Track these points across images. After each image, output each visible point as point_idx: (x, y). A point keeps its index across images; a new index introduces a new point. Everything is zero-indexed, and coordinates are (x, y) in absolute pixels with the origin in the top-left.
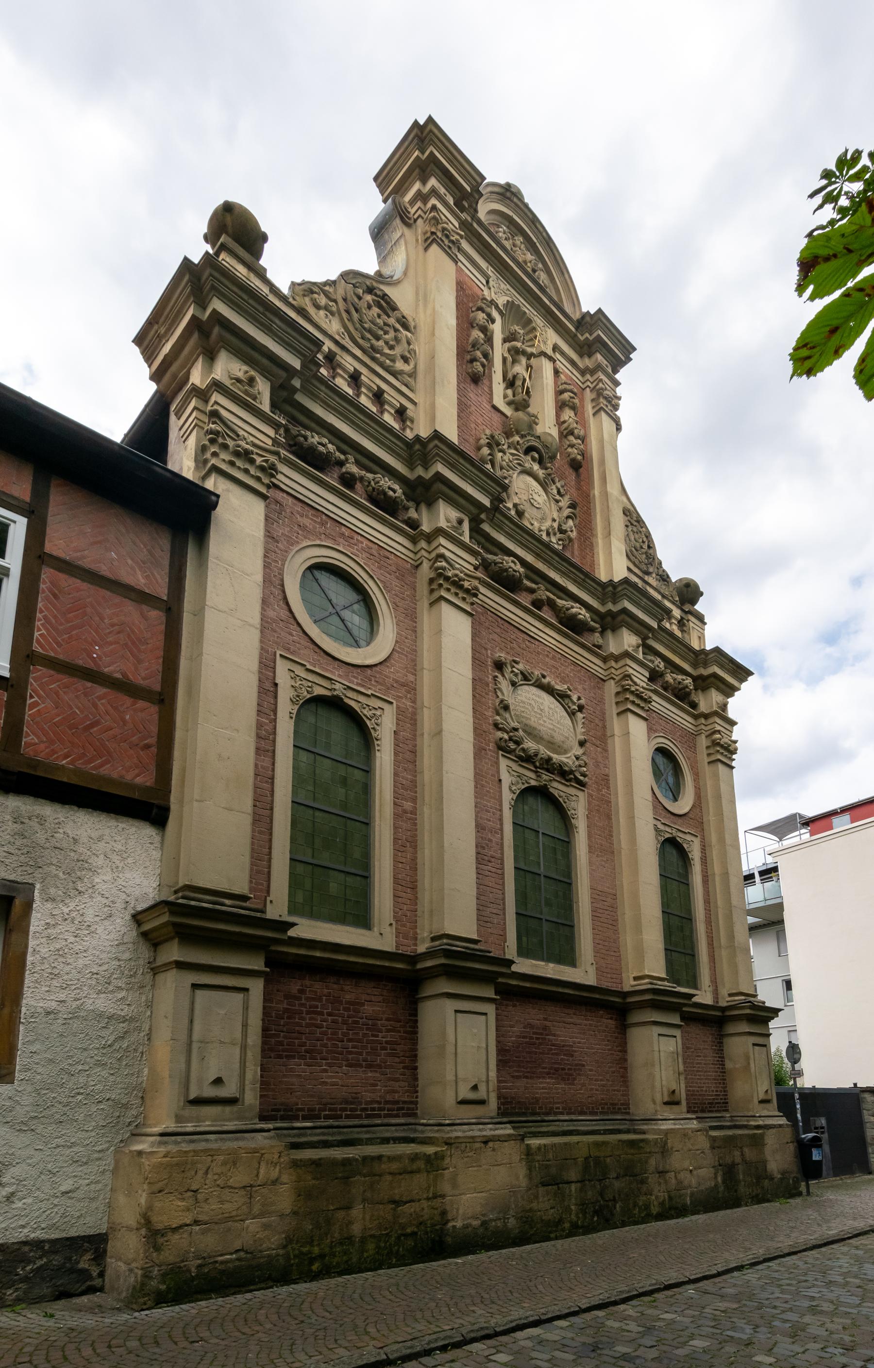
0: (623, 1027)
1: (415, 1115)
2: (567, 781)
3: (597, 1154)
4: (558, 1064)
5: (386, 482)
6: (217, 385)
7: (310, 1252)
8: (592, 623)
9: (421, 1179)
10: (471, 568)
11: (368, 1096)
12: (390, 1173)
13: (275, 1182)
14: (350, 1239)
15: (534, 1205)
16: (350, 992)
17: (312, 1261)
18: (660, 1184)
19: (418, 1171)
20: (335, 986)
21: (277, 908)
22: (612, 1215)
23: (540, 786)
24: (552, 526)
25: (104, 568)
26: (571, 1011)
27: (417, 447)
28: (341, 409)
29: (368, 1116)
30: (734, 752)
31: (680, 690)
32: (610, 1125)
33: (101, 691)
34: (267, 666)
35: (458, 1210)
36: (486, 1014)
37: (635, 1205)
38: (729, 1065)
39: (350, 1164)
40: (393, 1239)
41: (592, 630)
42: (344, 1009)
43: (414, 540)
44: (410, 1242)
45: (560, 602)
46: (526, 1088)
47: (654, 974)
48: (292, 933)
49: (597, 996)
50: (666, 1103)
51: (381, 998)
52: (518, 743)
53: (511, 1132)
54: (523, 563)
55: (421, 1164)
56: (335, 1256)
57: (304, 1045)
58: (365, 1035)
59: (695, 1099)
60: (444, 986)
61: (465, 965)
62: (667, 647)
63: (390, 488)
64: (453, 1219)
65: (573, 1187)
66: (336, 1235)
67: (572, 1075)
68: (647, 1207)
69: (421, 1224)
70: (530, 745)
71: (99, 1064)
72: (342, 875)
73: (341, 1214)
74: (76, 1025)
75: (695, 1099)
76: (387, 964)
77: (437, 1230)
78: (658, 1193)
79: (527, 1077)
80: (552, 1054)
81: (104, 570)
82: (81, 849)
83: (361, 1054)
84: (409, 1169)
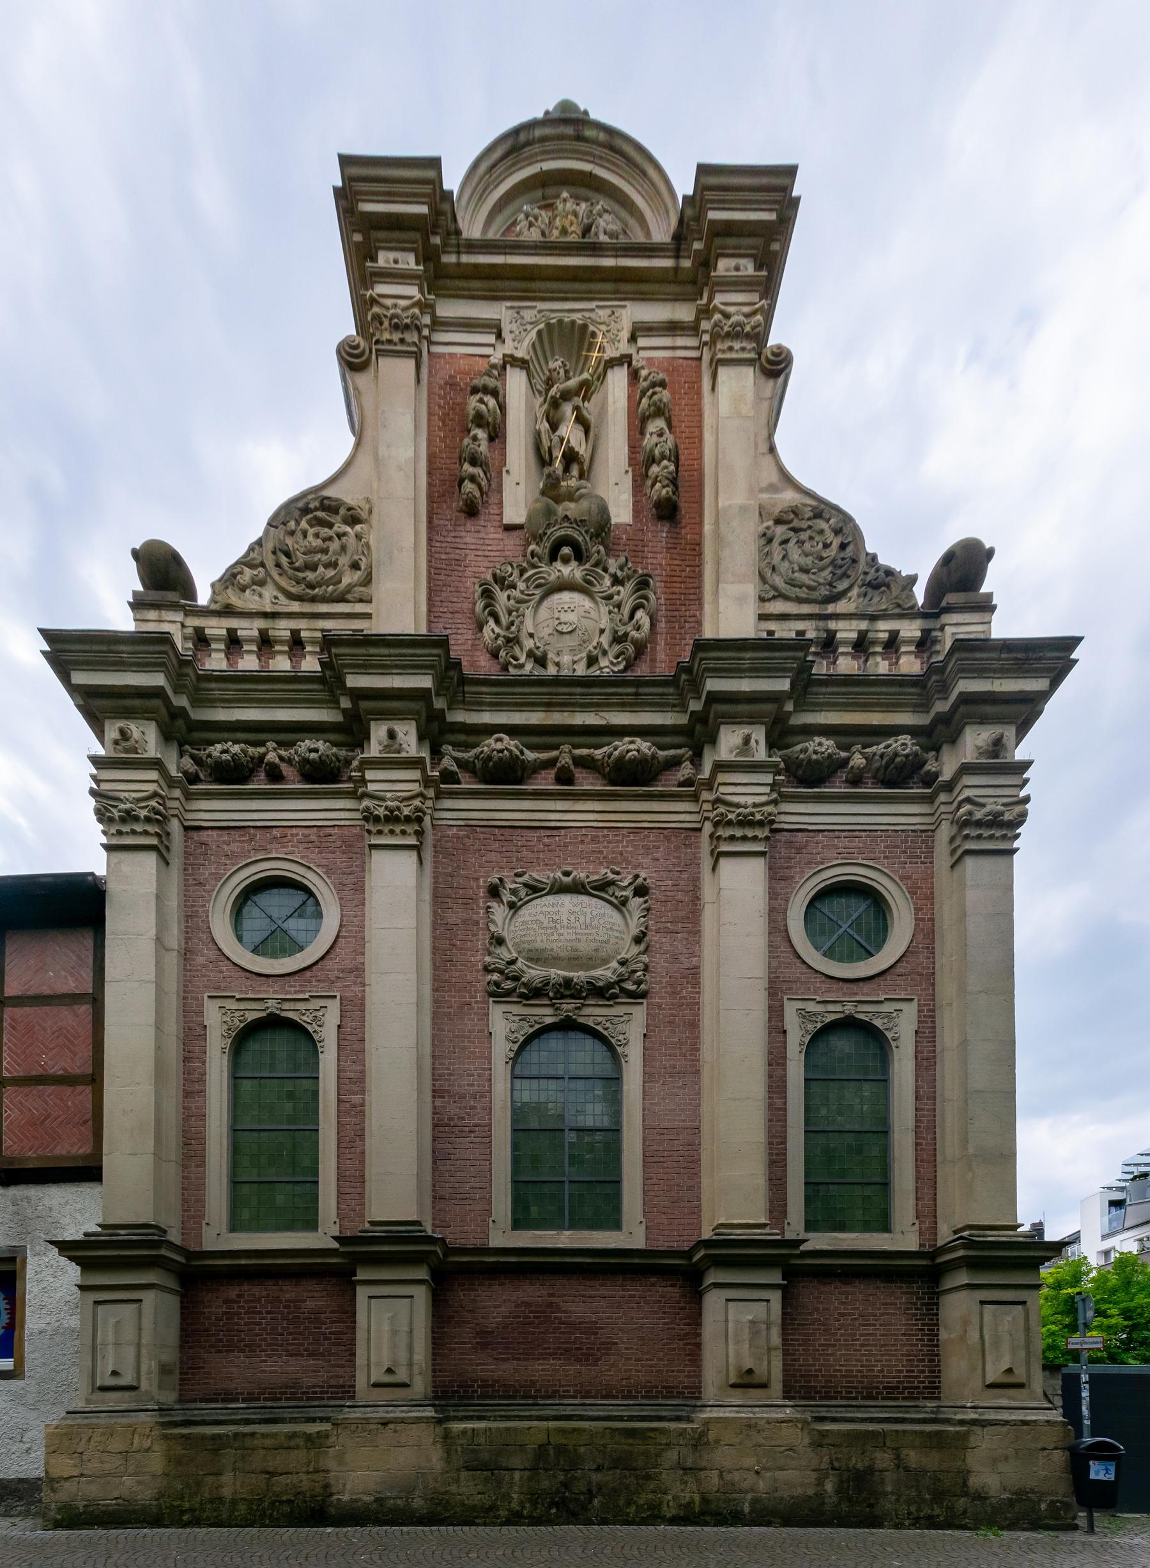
1: (699, 1398)
2: (608, 999)
7: (180, 1506)
8: (662, 754)
11: (311, 1381)
13: (148, 1450)
14: (220, 1500)
15: (453, 1488)
16: (289, 1291)
17: (183, 1512)
19: (297, 1447)
23: (562, 1021)
24: (599, 644)
25: (45, 988)
26: (597, 1283)
28: (240, 695)
29: (308, 1399)
33: (50, 1089)
34: (775, 1013)
35: (344, 1485)
41: (674, 763)
43: (695, 797)
44: (286, 1509)
45: (598, 753)
46: (516, 1370)
47: (735, 1222)
49: (637, 1261)
50: (733, 1386)
52: (516, 979)
53: (433, 1414)
54: (512, 731)
55: (301, 1442)
58: (306, 1328)
60: (963, 1277)
62: (497, 706)
63: (311, 750)
65: (517, 1475)
70: (534, 974)
71: (74, 1364)
72: (290, 1186)
73: (210, 1479)
74: (57, 1339)
76: (319, 1261)
78: (680, 1491)
81: (46, 991)
82: (55, 1214)
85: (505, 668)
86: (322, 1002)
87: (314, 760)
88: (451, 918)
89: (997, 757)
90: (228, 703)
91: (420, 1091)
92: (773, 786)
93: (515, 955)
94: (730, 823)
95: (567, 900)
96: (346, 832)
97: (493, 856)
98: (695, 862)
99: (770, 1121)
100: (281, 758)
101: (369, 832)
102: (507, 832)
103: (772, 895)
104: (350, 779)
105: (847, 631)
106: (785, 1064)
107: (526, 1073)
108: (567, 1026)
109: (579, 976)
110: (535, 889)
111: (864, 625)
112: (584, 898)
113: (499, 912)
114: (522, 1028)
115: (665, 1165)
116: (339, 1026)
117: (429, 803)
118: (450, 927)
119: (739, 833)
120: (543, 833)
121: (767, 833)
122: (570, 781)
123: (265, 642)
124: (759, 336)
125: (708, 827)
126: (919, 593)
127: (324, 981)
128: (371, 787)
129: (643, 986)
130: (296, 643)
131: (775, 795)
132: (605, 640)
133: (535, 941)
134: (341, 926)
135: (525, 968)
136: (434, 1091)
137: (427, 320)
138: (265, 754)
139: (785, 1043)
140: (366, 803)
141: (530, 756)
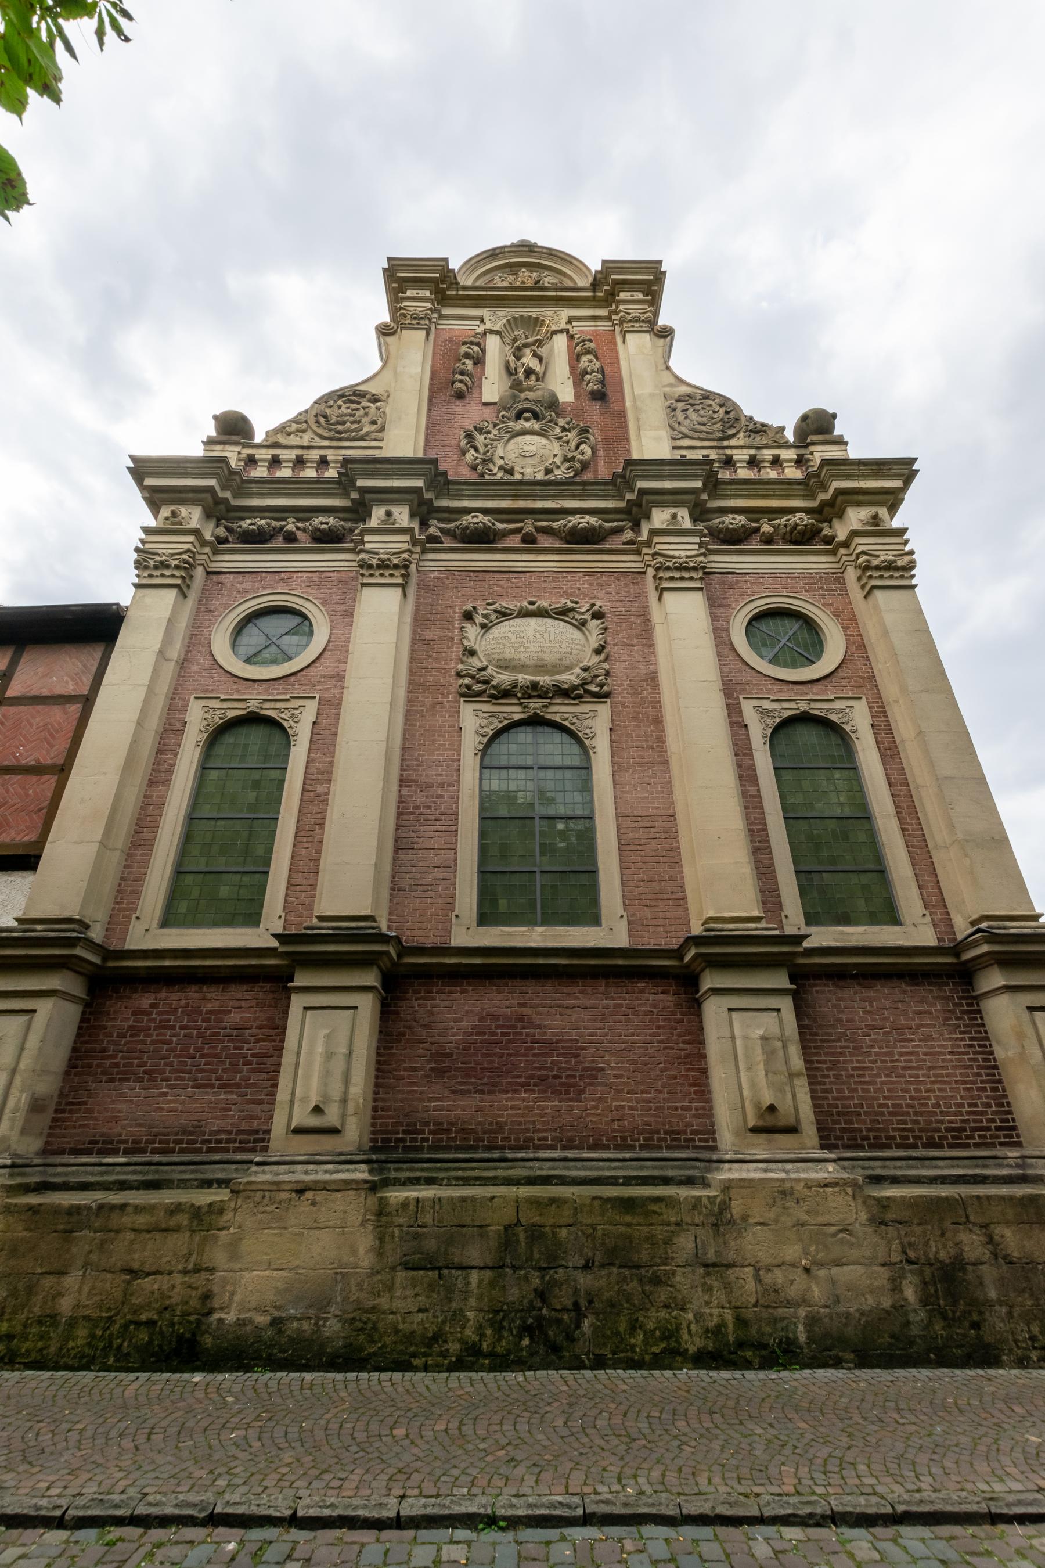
0: (693, 1004)
1: (714, 1148)
2: (574, 699)
3: (537, 1219)
4: (547, 1069)
5: (318, 521)
6: (854, 533)
8: (606, 525)
9: (179, 1242)
10: (697, 547)
11: (215, 1124)
12: (134, 1230)
14: (53, 1318)
15: (383, 1302)
16: (213, 998)
18: (709, 1289)
19: (177, 1229)
20: (196, 995)
21: (794, 921)
22: (571, 1338)
23: (529, 717)
27: (343, 479)
28: (273, 491)
30: (911, 566)
31: (791, 533)
32: (654, 1168)
34: (734, 711)
35: (232, 1294)
36: (778, 1010)
37: (634, 1326)
38: (999, 1053)
39: (79, 1214)
40: (117, 1326)
41: (620, 530)
42: (203, 1021)
43: (638, 552)
44: (144, 1336)
46: (479, 1108)
47: (726, 915)
48: (805, 944)
50: (755, 1130)
51: (253, 1003)
54: (486, 511)
55: (183, 1219)
56: (27, 1339)
57: (144, 1064)
59: (899, 1122)
61: (728, 951)
64: (222, 1309)
65: (474, 1276)
66: (36, 1310)
67: (574, 1085)
68: (670, 1333)
69: (166, 1309)
70: (503, 678)
73: (48, 1282)
75: (899, 1122)
77: (190, 1322)
79: (482, 1092)
80: (534, 1055)
83: (215, 1071)
84: (163, 1226)
85: (482, 475)
86: (301, 702)
87: (324, 530)
88: (429, 635)
89: (877, 525)
90: (729, 497)
91: (386, 780)
92: (701, 544)
93: (485, 663)
94: (668, 568)
95: (533, 622)
96: (343, 575)
97: (468, 591)
98: (643, 594)
99: (746, 808)
100: (298, 528)
101: (362, 575)
102: (481, 575)
103: (714, 618)
104: (352, 541)
105: (741, 455)
106: (751, 755)
107: (496, 764)
108: (535, 721)
109: (545, 680)
110: (504, 615)
111: (753, 452)
112: (549, 621)
113: (472, 631)
114: (491, 723)
115: (643, 853)
116: (314, 723)
117: (416, 556)
118: (428, 643)
119: (677, 575)
120: (511, 575)
121: (701, 574)
122: (534, 541)
123: (300, 462)
124: (652, 322)
125: (651, 572)
126: (790, 436)
127: (306, 685)
128: (367, 546)
129: (605, 688)
130: (323, 462)
131: (703, 550)
132: (558, 461)
133: (504, 652)
134: (329, 641)
135: (495, 674)
136: (401, 781)
137: (436, 315)
138: (285, 526)
139: (748, 735)
140: (362, 556)
141: (500, 526)
